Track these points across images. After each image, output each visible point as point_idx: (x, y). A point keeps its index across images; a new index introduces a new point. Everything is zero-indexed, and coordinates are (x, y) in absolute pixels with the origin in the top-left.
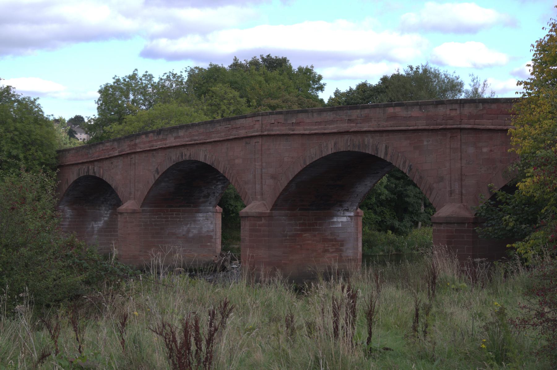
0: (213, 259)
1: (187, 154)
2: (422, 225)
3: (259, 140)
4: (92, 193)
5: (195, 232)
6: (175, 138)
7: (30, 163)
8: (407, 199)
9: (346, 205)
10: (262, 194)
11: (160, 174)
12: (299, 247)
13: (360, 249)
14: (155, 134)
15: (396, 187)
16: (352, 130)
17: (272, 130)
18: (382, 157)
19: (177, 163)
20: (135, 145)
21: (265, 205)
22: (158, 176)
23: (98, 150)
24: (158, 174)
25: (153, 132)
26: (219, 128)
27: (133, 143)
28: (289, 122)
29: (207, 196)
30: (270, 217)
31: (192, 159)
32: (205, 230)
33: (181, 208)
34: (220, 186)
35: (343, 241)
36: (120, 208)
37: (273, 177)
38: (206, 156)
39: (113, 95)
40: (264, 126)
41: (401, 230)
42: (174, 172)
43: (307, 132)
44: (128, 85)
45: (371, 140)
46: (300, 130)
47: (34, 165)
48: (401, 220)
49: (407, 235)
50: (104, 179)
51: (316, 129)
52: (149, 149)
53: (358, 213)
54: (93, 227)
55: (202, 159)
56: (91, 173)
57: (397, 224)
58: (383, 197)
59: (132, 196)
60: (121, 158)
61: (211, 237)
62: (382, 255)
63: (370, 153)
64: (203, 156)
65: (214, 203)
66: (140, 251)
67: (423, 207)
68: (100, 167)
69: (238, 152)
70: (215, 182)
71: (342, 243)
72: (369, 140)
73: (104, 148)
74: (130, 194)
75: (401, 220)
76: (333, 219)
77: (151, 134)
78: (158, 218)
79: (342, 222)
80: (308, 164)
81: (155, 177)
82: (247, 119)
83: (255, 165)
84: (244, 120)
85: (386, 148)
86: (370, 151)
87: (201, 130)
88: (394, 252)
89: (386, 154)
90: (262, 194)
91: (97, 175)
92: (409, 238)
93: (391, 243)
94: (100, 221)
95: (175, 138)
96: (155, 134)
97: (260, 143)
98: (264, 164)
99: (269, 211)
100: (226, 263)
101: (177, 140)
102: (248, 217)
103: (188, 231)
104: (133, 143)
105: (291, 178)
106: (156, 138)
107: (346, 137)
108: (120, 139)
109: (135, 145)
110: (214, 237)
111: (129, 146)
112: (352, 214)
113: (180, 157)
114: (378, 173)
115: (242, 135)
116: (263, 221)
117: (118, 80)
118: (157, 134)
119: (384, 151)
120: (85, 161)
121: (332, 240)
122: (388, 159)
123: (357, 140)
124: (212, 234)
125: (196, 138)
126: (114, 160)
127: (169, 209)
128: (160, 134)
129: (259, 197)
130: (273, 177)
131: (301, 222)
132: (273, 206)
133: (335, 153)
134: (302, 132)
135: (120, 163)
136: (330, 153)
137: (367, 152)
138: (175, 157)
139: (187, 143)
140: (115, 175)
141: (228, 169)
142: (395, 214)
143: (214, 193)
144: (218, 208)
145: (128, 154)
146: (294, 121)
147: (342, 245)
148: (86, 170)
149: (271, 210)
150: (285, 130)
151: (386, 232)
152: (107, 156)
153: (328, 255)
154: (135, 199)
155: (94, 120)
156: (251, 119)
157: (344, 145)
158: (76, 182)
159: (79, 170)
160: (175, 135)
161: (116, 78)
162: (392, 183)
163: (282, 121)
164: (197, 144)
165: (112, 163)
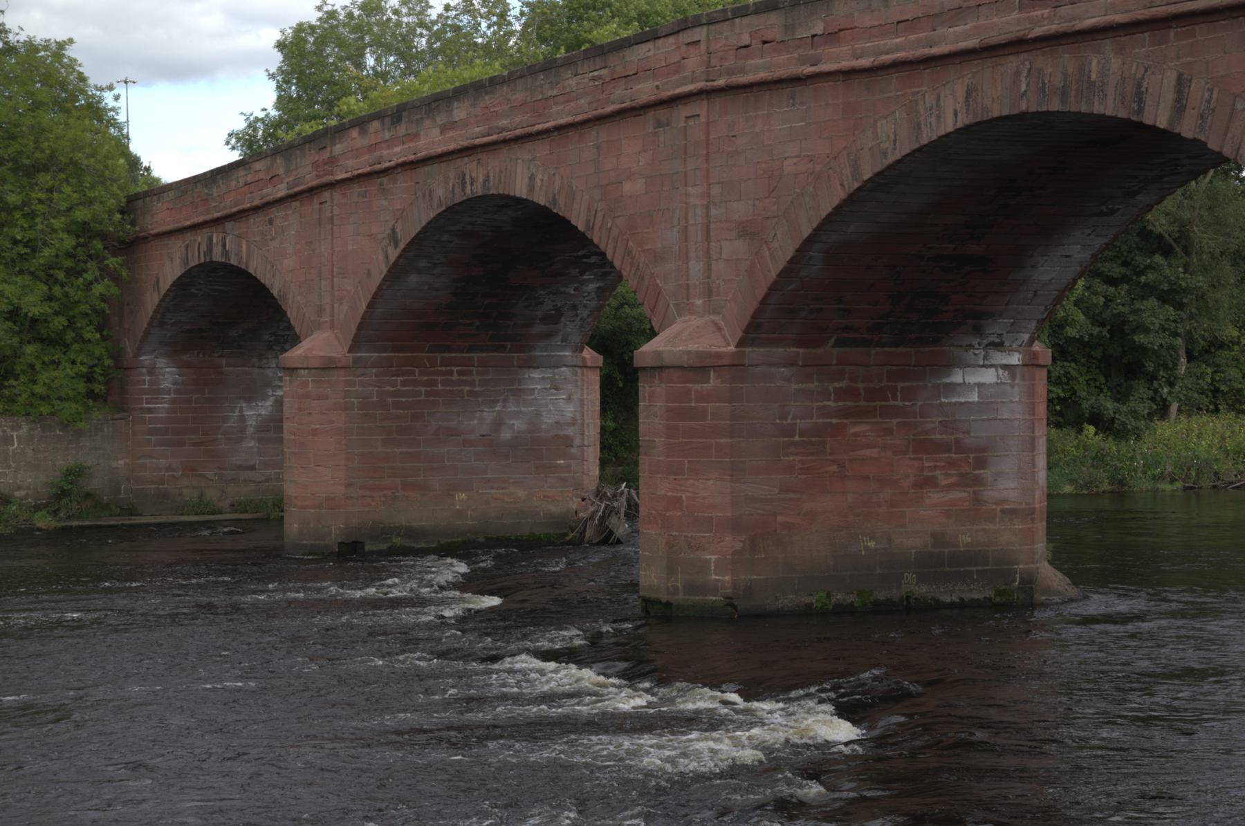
0: (573, 506)
1: (482, 176)
2: (1180, 411)
3: (700, 108)
4: (232, 316)
5: (519, 425)
6: (444, 129)
7: (40, 227)
8: (1140, 338)
9: (995, 329)
10: (710, 293)
11: (402, 245)
12: (835, 468)
13: (1042, 476)
14: (387, 121)
15: (1106, 306)
16: (1038, 31)
17: (743, 71)
18: (1162, 123)
19: (448, 209)
20: (332, 160)
21: (719, 329)
22: (399, 251)
23: (233, 184)
24: (396, 246)
25: (378, 116)
26: (573, 82)
27: (325, 155)
28: (802, 33)
29: (554, 318)
30: (736, 367)
31: (493, 191)
32: (548, 419)
33: (475, 355)
34: (591, 287)
35: (984, 450)
36: (286, 354)
37: (747, 231)
38: (532, 178)
39: (319, 52)
40: (714, 61)
41: (1124, 424)
42: (445, 237)
43: (865, 62)
44: (359, 28)
45: (1115, 64)
46: (837, 58)
47: (54, 231)
48: (1121, 396)
49: (1138, 438)
50: (251, 271)
51: (898, 48)
52: (368, 169)
53: (1035, 355)
54: (242, 418)
55: (520, 191)
56: (217, 257)
57: (1109, 406)
58: (1071, 332)
59: (326, 318)
60: (296, 204)
61: (567, 441)
62: (1070, 495)
63: (1109, 113)
64: (526, 180)
65: (576, 338)
66: (349, 485)
67: (1183, 360)
68: (239, 236)
69: (631, 150)
70: (575, 272)
71: (981, 456)
72: (1105, 63)
73: (249, 179)
74: (320, 310)
75: (1121, 396)
76: (949, 375)
77: (375, 125)
78: (403, 384)
79: (980, 385)
80: (867, 175)
81: (387, 257)
82: (660, 42)
83: (687, 195)
84: (650, 45)
85: (1182, 84)
86: (1109, 106)
87: (519, 96)
88: (1106, 486)
89: (1179, 108)
90: (710, 293)
91: (234, 262)
92: (1146, 447)
93: (1100, 459)
94: (265, 398)
95: (444, 129)
96: (387, 121)
97: (703, 119)
98: (716, 190)
99: (732, 348)
100: (613, 521)
101: (450, 134)
102: (661, 368)
103: (498, 424)
104: (325, 155)
105: (806, 231)
106: (387, 135)
107: (1012, 63)
108: (291, 147)
109: (332, 160)
110: (577, 442)
111: (316, 165)
112: (1015, 359)
113: (457, 190)
114: (1112, 212)
115: (644, 98)
116: (713, 382)
117: (332, 14)
118: (393, 123)
119: (1169, 97)
120: (200, 219)
121: (944, 447)
122: (1187, 129)
123: (1056, 68)
124: (570, 431)
125: (504, 122)
126: (277, 213)
127: (439, 356)
128: (399, 120)
129: (699, 302)
130: (747, 231)
131: (843, 384)
132: (746, 332)
133: (967, 129)
134: (845, 64)
135: (290, 220)
136: (950, 129)
137: (1098, 109)
138: (443, 188)
139: (477, 141)
140: (277, 256)
141: (600, 215)
142: (1102, 380)
143: (574, 307)
144: (588, 353)
145: (312, 190)
146: (819, 29)
147: (981, 463)
148: (203, 248)
149: (737, 346)
150: (786, 64)
151: (1080, 431)
152: (257, 202)
153: (934, 497)
154: (332, 327)
155: (262, 120)
156: (672, 39)
157: (1002, 92)
158: (183, 285)
159: (187, 247)
160: (441, 119)
161: (326, 8)
162: (1096, 293)
163: (776, 34)
164: (506, 142)
165: (271, 222)
